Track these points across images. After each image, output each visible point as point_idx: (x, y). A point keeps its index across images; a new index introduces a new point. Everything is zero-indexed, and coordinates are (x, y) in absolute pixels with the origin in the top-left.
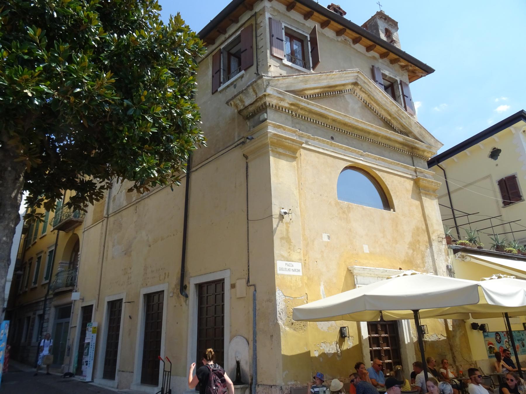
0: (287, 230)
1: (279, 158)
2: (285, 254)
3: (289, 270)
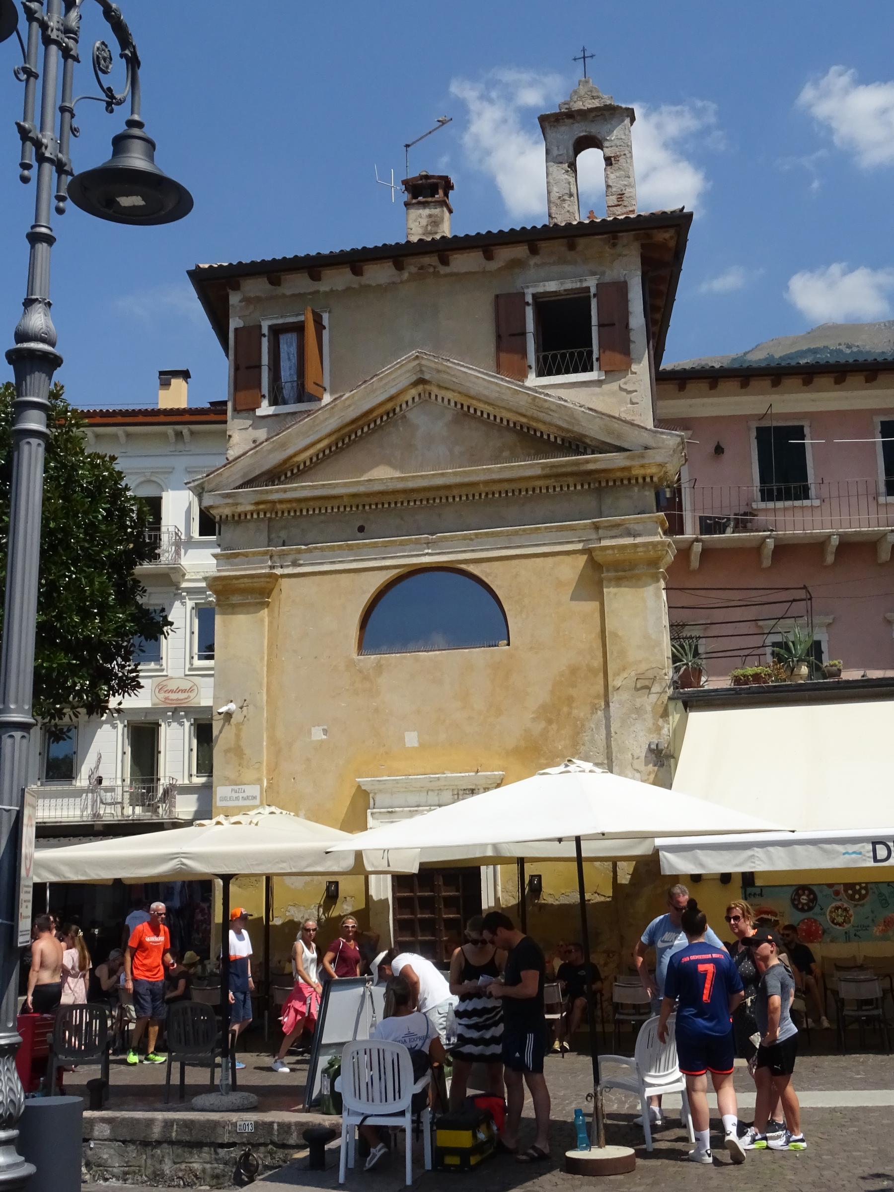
0: (238, 736)
1: (233, 614)
2: (232, 775)
3: (237, 798)
